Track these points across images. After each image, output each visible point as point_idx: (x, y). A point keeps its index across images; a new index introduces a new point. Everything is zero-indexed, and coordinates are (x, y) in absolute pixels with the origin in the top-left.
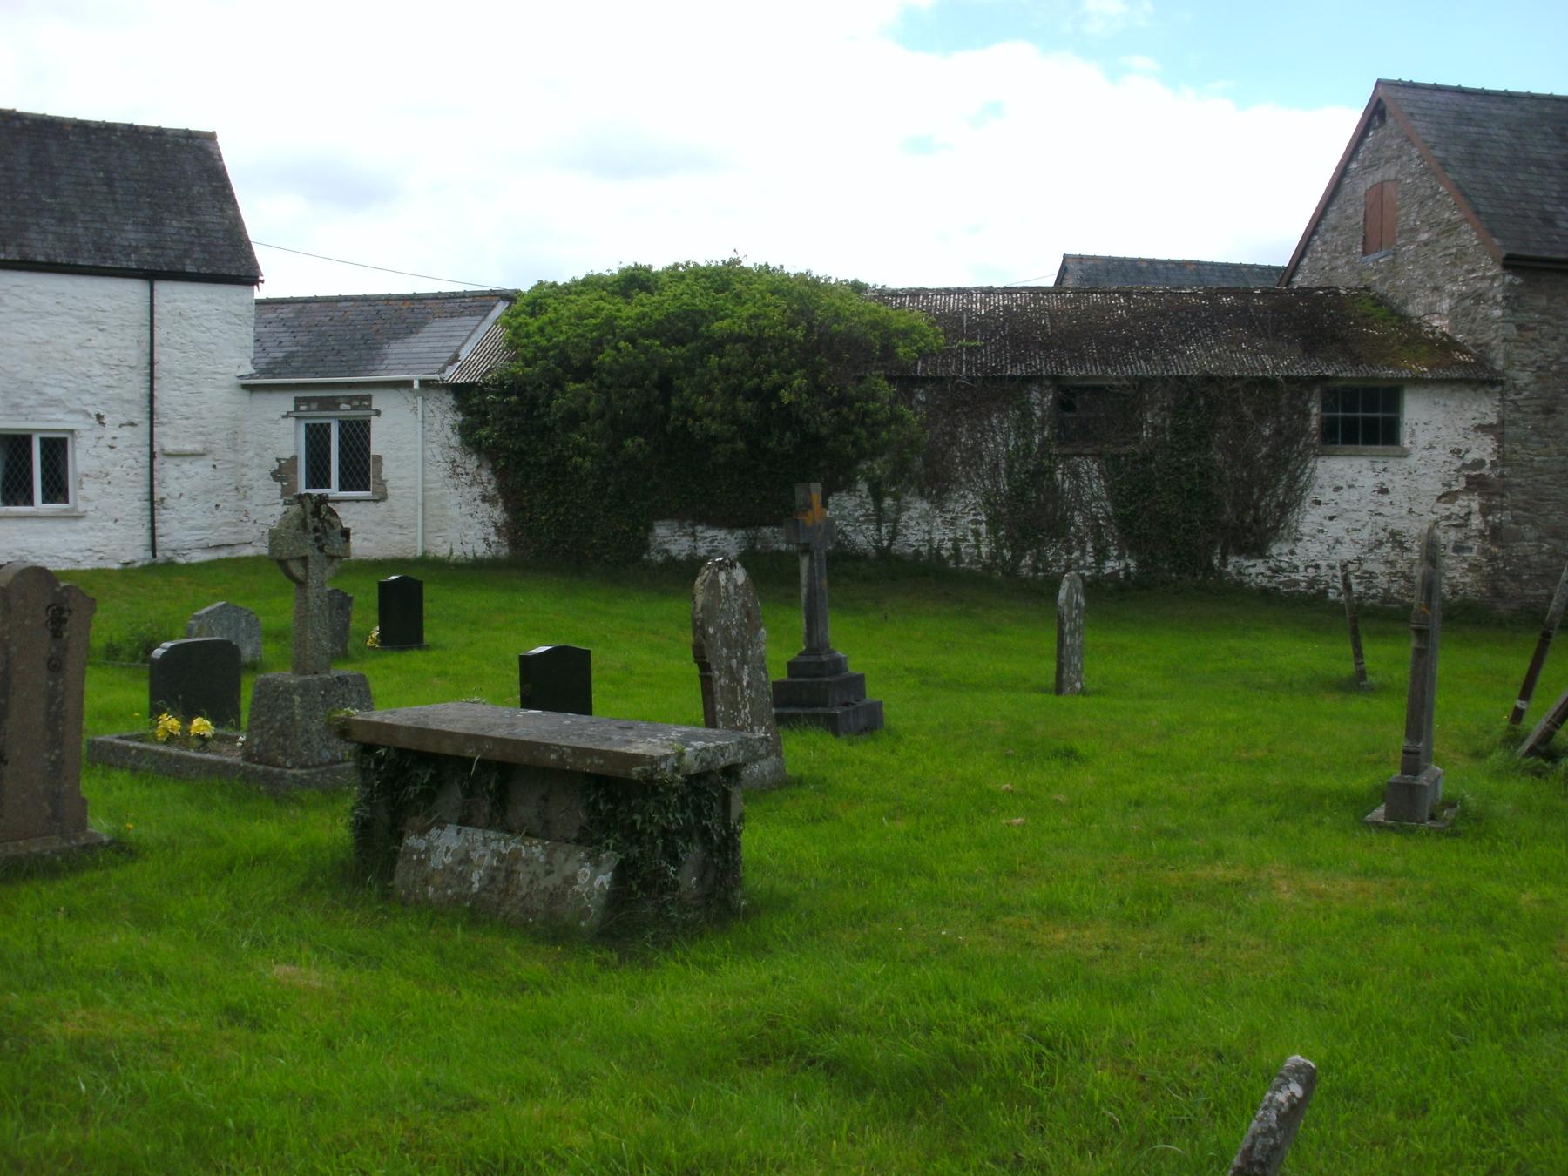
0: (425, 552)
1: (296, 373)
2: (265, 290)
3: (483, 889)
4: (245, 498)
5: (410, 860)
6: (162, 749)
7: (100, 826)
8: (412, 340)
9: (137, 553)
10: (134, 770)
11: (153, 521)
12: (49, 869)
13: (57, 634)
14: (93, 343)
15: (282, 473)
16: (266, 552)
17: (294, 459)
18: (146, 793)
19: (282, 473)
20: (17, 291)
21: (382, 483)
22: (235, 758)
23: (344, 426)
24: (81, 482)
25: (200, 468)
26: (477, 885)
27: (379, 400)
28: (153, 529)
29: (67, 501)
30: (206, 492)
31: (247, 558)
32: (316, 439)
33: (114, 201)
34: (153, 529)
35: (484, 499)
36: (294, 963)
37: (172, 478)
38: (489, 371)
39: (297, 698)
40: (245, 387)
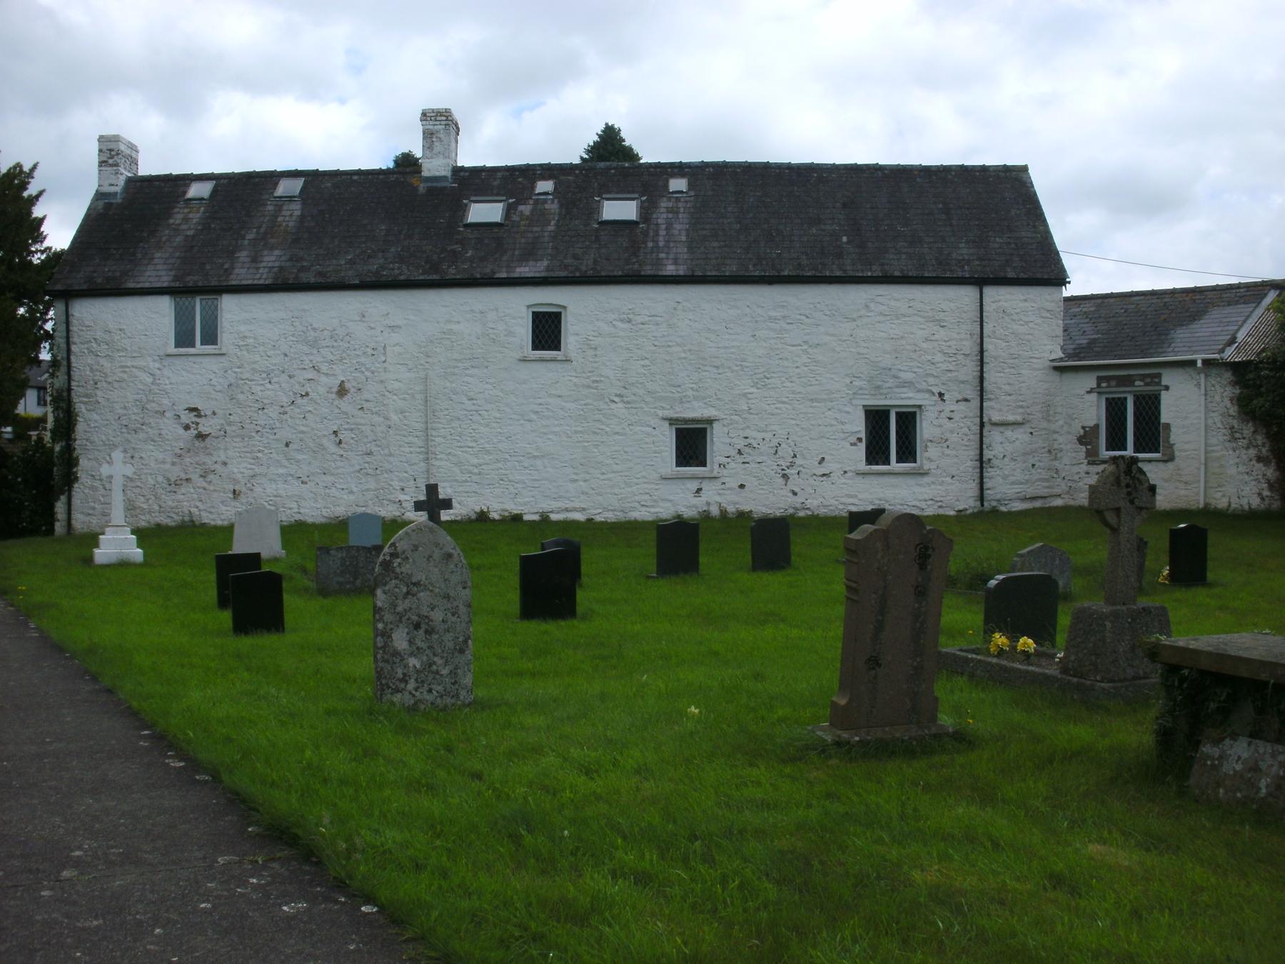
0: (1206, 505)
1: (1097, 357)
2: (1073, 289)
3: (1270, 794)
4: (1056, 459)
5: (1205, 764)
6: (995, 660)
7: (946, 720)
8: (1195, 326)
9: (968, 502)
10: (972, 676)
11: (982, 477)
12: (909, 751)
13: (922, 566)
14: (936, 337)
15: (1088, 437)
16: (1085, 502)
17: (1097, 426)
18: (982, 695)
19: (1088, 437)
20: (880, 299)
21: (1171, 446)
22: (1053, 671)
23: (1138, 399)
24: (926, 447)
25: (1020, 435)
26: (1264, 791)
27: (1168, 378)
28: (982, 483)
29: (915, 462)
30: (1025, 454)
31: (1057, 507)
32: (1115, 411)
33: (951, 225)
34: (982, 483)
35: (1259, 459)
36: (1105, 843)
37: (998, 443)
38: (1263, 350)
39: (1108, 624)
40: (1056, 368)
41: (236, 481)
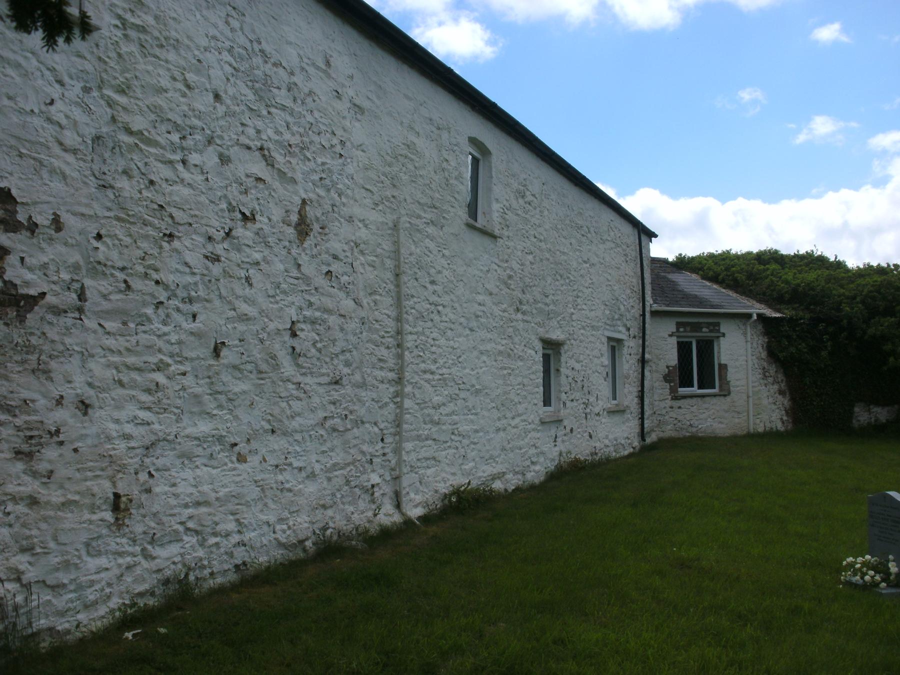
32: (684, 349)
41: (114, 465)
